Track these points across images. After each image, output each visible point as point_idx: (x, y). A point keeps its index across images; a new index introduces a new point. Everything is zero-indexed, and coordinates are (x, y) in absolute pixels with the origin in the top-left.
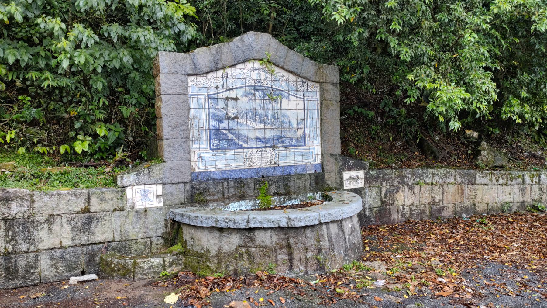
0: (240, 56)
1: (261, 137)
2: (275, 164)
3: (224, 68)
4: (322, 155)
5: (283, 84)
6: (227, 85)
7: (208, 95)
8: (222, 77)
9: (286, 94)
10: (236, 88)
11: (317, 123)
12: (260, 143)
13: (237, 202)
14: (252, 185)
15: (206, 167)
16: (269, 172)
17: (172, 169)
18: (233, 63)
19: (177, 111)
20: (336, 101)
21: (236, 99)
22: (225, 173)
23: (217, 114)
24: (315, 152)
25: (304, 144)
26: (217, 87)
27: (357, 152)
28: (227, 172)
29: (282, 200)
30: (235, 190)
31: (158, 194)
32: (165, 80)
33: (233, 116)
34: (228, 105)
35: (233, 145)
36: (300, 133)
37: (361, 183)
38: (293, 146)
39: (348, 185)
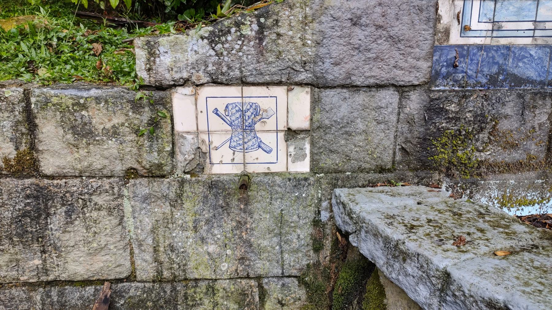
17: (355, 22)
31: (294, 126)
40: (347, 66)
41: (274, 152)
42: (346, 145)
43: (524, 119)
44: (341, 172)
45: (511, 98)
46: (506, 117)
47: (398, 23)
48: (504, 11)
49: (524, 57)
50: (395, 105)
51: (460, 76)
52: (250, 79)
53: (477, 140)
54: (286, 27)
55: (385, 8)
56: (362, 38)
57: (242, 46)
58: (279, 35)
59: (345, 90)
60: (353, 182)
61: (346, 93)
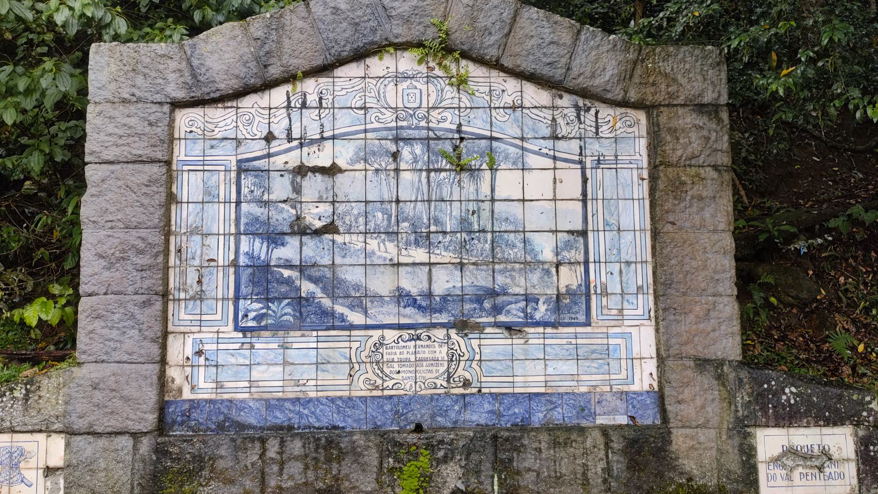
0: (344, 37)
1: (414, 291)
2: (467, 384)
3: (290, 78)
4: (661, 360)
5: (500, 116)
6: (304, 129)
7: (239, 161)
8: (288, 107)
9: (512, 150)
10: (334, 138)
11: (637, 245)
12: (409, 311)
14: (372, 457)
15: (219, 385)
17: (95, 387)
18: (318, 62)
19: (128, 210)
20: (715, 167)
21: (332, 171)
22: (281, 408)
23: (264, 218)
25: (582, 318)
26: (269, 138)
27: (861, 348)
28: (287, 405)
30: (306, 467)
31: (52, 464)
32: (98, 121)
33: (318, 224)
34: (305, 191)
35: (312, 316)
36: (569, 278)
37: (841, 476)
38: (537, 324)
40: (89, 419)
41: (34, 486)
42: (91, 481)
43: (237, 459)
46: (221, 457)
49: (245, 408)
50: (130, 447)
51: (193, 423)
52: (17, 429)
53: (201, 477)
54: (45, 391)
57: (13, 405)
58: (40, 397)
61: (90, 438)
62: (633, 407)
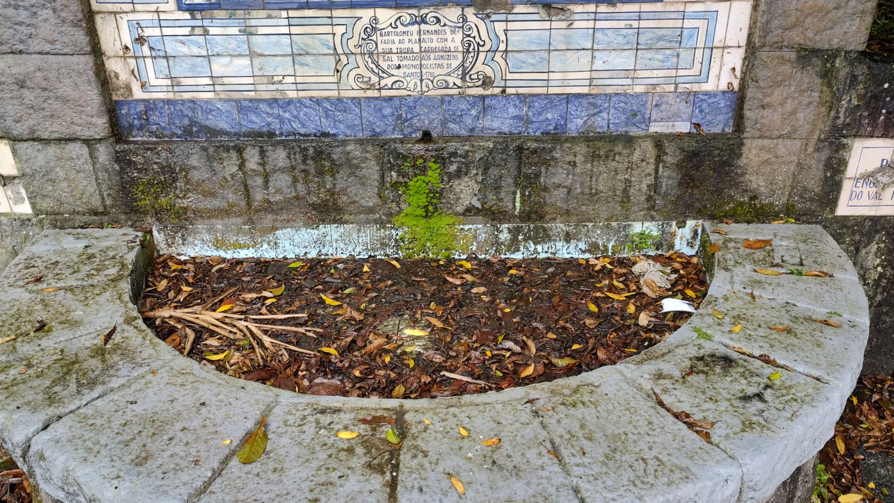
2: (487, 82)
4: (752, 49)
13: (307, 225)
14: (372, 170)
15: (175, 82)
16: (458, 119)
17: (22, 85)
22: (256, 111)
24: (710, 34)
29: (505, 236)
30: (295, 180)
39: (865, 200)
40: (28, 123)
44: (58, 214)
45: (194, 151)
47: (61, 86)
48: (177, 67)
49: (212, 110)
55: (45, 73)
56: (33, 98)
59: (36, 143)
60: (70, 223)
62: (701, 111)
